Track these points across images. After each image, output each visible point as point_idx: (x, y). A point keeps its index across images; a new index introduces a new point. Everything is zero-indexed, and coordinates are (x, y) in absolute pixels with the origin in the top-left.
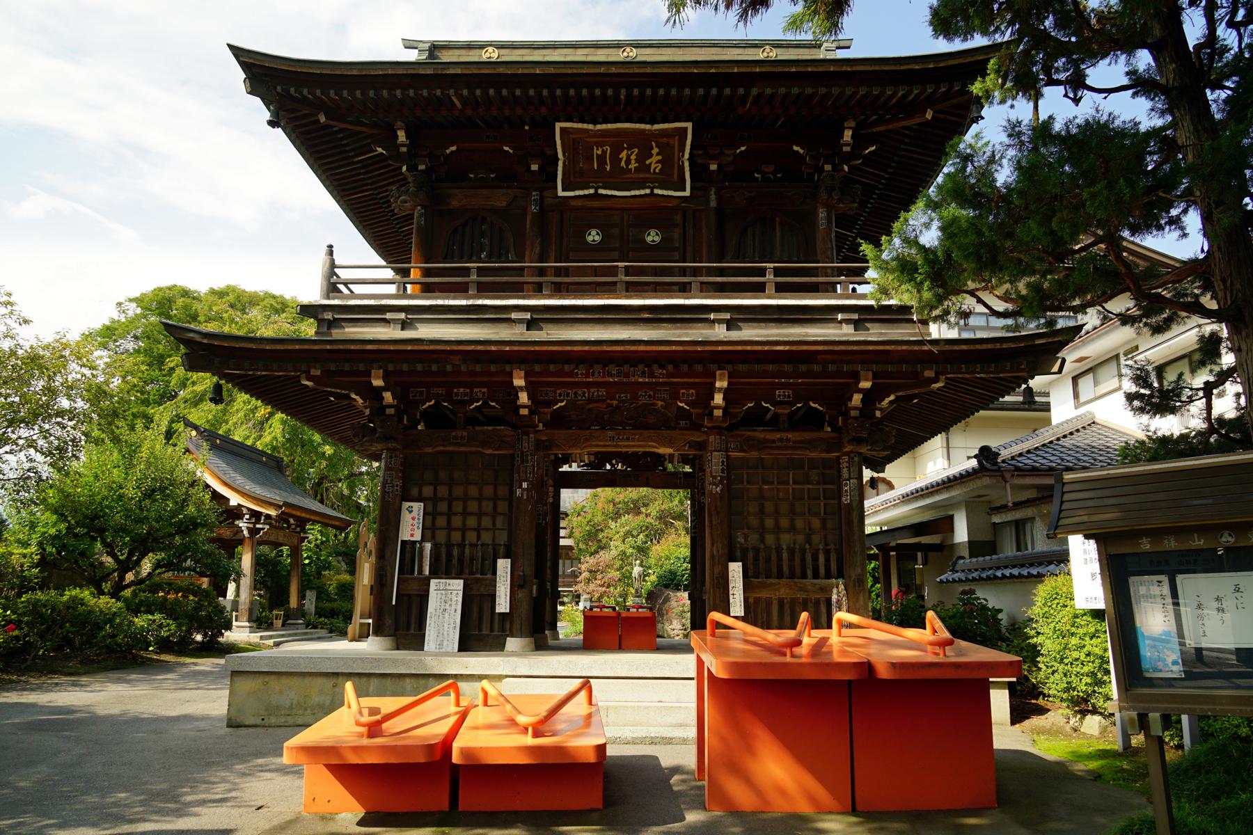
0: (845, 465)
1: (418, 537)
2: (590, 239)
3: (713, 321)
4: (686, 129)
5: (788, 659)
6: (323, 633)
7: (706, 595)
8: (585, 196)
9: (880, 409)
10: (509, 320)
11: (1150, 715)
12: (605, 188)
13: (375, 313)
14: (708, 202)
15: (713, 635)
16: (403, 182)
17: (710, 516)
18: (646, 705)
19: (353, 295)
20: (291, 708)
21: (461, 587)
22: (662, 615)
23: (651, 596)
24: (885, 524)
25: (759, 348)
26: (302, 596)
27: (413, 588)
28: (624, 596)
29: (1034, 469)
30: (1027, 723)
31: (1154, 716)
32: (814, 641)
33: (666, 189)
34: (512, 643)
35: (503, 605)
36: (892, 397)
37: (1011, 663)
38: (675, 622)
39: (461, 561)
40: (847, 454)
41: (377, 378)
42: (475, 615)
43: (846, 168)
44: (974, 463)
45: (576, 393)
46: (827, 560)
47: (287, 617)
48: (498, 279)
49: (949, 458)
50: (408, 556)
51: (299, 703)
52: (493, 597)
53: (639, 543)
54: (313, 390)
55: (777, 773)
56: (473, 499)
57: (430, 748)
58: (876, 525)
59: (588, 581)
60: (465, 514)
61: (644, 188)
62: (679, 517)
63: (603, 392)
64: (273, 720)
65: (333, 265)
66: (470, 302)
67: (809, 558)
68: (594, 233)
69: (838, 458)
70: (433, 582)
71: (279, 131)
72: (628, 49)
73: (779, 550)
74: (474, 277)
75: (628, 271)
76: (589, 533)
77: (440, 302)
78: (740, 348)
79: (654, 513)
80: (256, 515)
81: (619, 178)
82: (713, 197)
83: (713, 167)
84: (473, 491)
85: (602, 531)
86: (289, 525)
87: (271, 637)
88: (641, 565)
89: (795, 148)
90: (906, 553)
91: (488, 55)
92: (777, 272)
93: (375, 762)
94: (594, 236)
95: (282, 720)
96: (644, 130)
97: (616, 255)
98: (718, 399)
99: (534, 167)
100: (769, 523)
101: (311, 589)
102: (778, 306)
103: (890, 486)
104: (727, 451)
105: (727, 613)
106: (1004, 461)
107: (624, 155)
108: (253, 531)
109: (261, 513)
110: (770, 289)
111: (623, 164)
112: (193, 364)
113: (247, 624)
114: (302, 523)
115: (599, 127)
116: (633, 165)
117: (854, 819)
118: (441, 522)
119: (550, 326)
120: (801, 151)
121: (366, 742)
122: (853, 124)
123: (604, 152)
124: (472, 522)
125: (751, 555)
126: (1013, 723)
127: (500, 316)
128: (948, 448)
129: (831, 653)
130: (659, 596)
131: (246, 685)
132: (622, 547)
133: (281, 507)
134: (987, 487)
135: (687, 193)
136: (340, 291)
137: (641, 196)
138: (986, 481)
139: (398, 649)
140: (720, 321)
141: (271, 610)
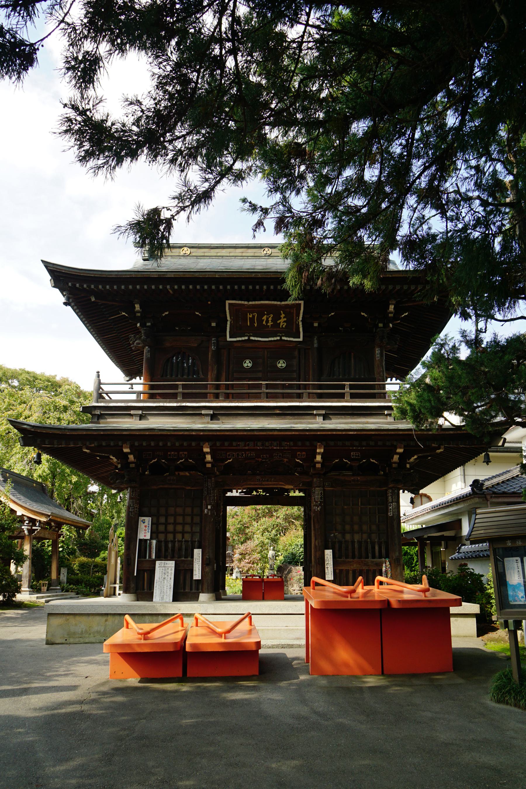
0: (390, 494)
1: (148, 537)
2: (245, 365)
3: (316, 415)
4: (300, 304)
5: (349, 599)
6: (73, 594)
7: (313, 568)
8: (242, 341)
9: (409, 463)
10: (201, 415)
11: (509, 621)
12: (254, 336)
13: (124, 411)
14: (313, 344)
15: (314, 589)
16: (137, 332)
17: (314, 524)
18: (280, 627)
19: (111, 401)
20: (82, 633)
21: (174, 565)
22: (287, 581)
23: (280, 569)
24: (424, 524)
25: (340, 433)
26: (59, 573)
27: (146, 566)
28: (263, 569)
29: (504, 493)
30: (486, 636)
31: (511, 621)
32: (364, 591)
33: (257, 337)
34: (203, 597)
35: (197, 575)
36: (415, 457)
37: (456, 600)
38: (295, 585)
39: (173, 550)
40: (391, 488)
41: (126, 448)
42: (182, 581)
43: (391, 325)
44: (468, 489)
45: (238, 454)
46: (380, 548)
47: (50, 585)
48: (194, 391)
49: (465, 482)
50: (143, 548)
51: (86, 631)
52: (192, 571)
53: (272, 536)
54: (89, 454)
55: (344, 654)
56: (180, 515)
57: (175, 644)
58: (417, 524)
59: (240, 560)
60: (175, 524)
61: (276, 336)
62: (297, 518)
63: (253, 454)
64: (72, 640)
65: (100, 383)
66: (179, 404)
67: (370, 546)
68: (247, 361)
69: (386, 490)
70: (158, 563)
71: (69, 308)
72: (266, 249)
73: (353, 542)
74: (180, 390)
75: (268, 386)
76: (240, 529)
77: (161, 404)
78: (330, 433)
79: (282, 516)
80: (32, 521)
81: (262, 331)
82: (316, 341)
83: (316, 325)
84: (179, 510)
85: (248, 527)
86: (51, 527)
87: (43, 597)
88: (274, 550)
89: (362, 314)
90: (436, 542)
91: (184, 252)
92: (351, 387)
93: (149, 651)
94: (248, 364)
95: (77, 640)
96: (276, 305)
97: (260, 375)
98: (319, 458)
99: (214, 324)
100: (348, 527)
101: (63, 567)
102: (352, 406)
103: (430, 499)
104: (323, 487)
105: (324, 578)
106: (487, 488)
107: (265, 318)
108: (31, 531)
109: (35, 520)
110: (347, 397)
111: (264, 323)
112: (26, 443)
113: (28, 589)
114: (59, 525)
115: (251, 303)
116: (270, 324)
117: (382, 677)
118: (162, 528)
119: (224, 418)
120: (366, 316)
121: (143, 641)
122: (394, 302)
123: (254, 316)
124: (179, 528)
125: (337, 546)
126: (478, 636)
127: (195, 412)
128: (464, 475)
129: (374, 596)
130: (285, 569)
131: (56, 621)
132: (262, 539)
133: (49, 516)
134: (477, 503)
135: (301, 339)
136: (104, 398)
137: (274, 341)
138: (477, 500)
139: (138, 601)
140: (319, 415)
141: (38, 581)
